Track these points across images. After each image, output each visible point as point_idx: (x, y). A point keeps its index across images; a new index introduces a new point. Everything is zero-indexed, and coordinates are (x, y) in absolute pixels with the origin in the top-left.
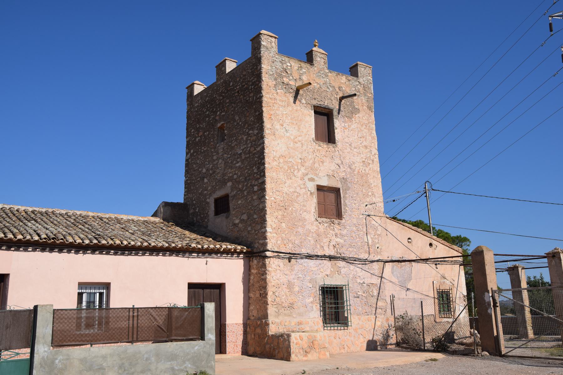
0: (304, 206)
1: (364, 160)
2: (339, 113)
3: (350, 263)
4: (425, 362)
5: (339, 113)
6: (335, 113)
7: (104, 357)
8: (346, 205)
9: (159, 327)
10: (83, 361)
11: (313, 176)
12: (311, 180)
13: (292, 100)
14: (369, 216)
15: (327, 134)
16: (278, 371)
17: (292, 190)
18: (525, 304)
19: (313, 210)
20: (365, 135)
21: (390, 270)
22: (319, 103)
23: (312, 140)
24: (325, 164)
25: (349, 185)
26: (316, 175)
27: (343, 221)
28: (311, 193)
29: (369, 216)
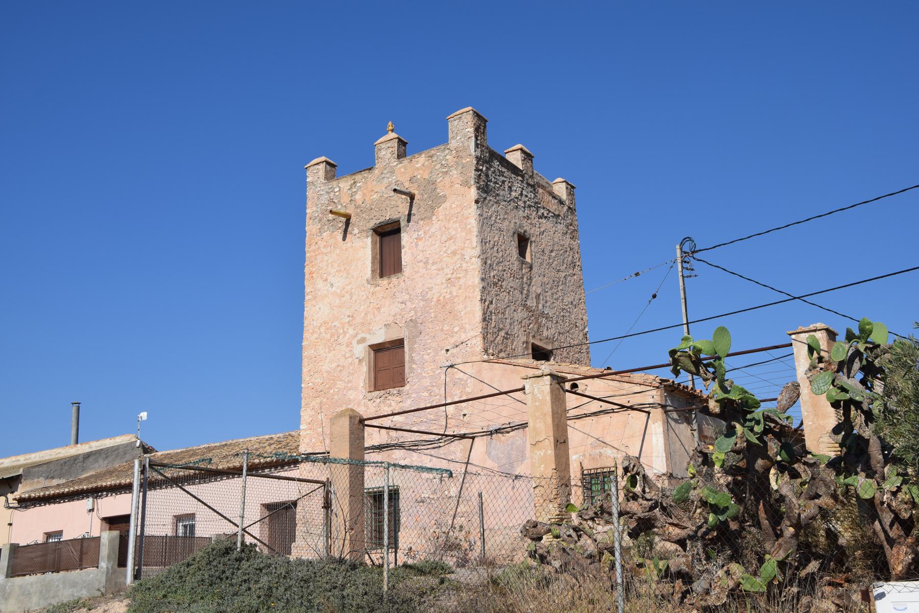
0: (349, 382)
1: (449, 276)
2: (409, 221)
3: (413, 450)
4: (137, 582)
5: (409, 221)
6: (403, 224)
7: (32, 584)
8: (412, 360)
9: (769, 600)
10: (21, 587)
11: (363, 335)
12: (363, 340)
13: (341, 236)
14: (452, 366)
15: (388, 262)
16: (36, 603)
17: (334, 365)
18: (822, 348)
19: (362, 384)
20: (453, 233)
21: (483, 449)
22: (378, 222)
23: (365, 282)
24: (382, 310)
25: (421, 328)
26: (369, 331)
27: (407, 387)
28: (360, 361)
29: (452, 366)
